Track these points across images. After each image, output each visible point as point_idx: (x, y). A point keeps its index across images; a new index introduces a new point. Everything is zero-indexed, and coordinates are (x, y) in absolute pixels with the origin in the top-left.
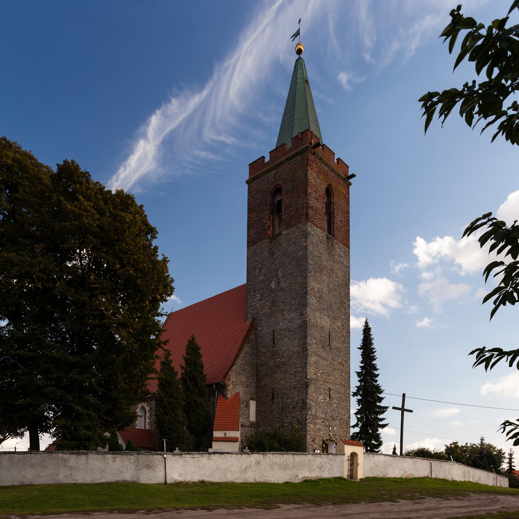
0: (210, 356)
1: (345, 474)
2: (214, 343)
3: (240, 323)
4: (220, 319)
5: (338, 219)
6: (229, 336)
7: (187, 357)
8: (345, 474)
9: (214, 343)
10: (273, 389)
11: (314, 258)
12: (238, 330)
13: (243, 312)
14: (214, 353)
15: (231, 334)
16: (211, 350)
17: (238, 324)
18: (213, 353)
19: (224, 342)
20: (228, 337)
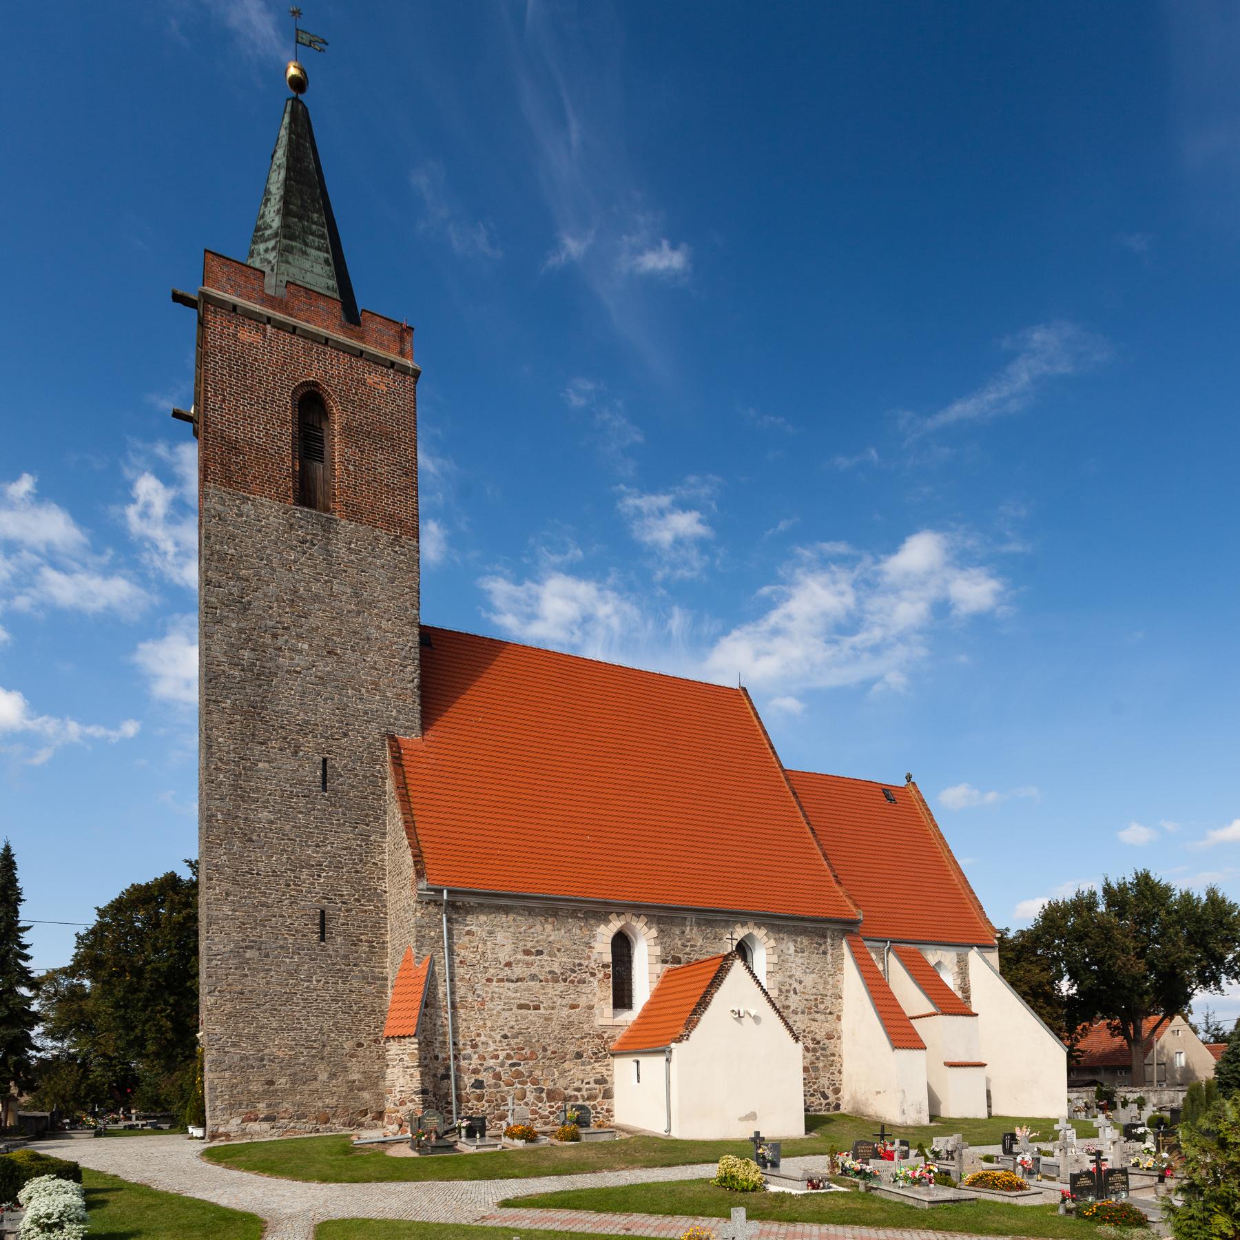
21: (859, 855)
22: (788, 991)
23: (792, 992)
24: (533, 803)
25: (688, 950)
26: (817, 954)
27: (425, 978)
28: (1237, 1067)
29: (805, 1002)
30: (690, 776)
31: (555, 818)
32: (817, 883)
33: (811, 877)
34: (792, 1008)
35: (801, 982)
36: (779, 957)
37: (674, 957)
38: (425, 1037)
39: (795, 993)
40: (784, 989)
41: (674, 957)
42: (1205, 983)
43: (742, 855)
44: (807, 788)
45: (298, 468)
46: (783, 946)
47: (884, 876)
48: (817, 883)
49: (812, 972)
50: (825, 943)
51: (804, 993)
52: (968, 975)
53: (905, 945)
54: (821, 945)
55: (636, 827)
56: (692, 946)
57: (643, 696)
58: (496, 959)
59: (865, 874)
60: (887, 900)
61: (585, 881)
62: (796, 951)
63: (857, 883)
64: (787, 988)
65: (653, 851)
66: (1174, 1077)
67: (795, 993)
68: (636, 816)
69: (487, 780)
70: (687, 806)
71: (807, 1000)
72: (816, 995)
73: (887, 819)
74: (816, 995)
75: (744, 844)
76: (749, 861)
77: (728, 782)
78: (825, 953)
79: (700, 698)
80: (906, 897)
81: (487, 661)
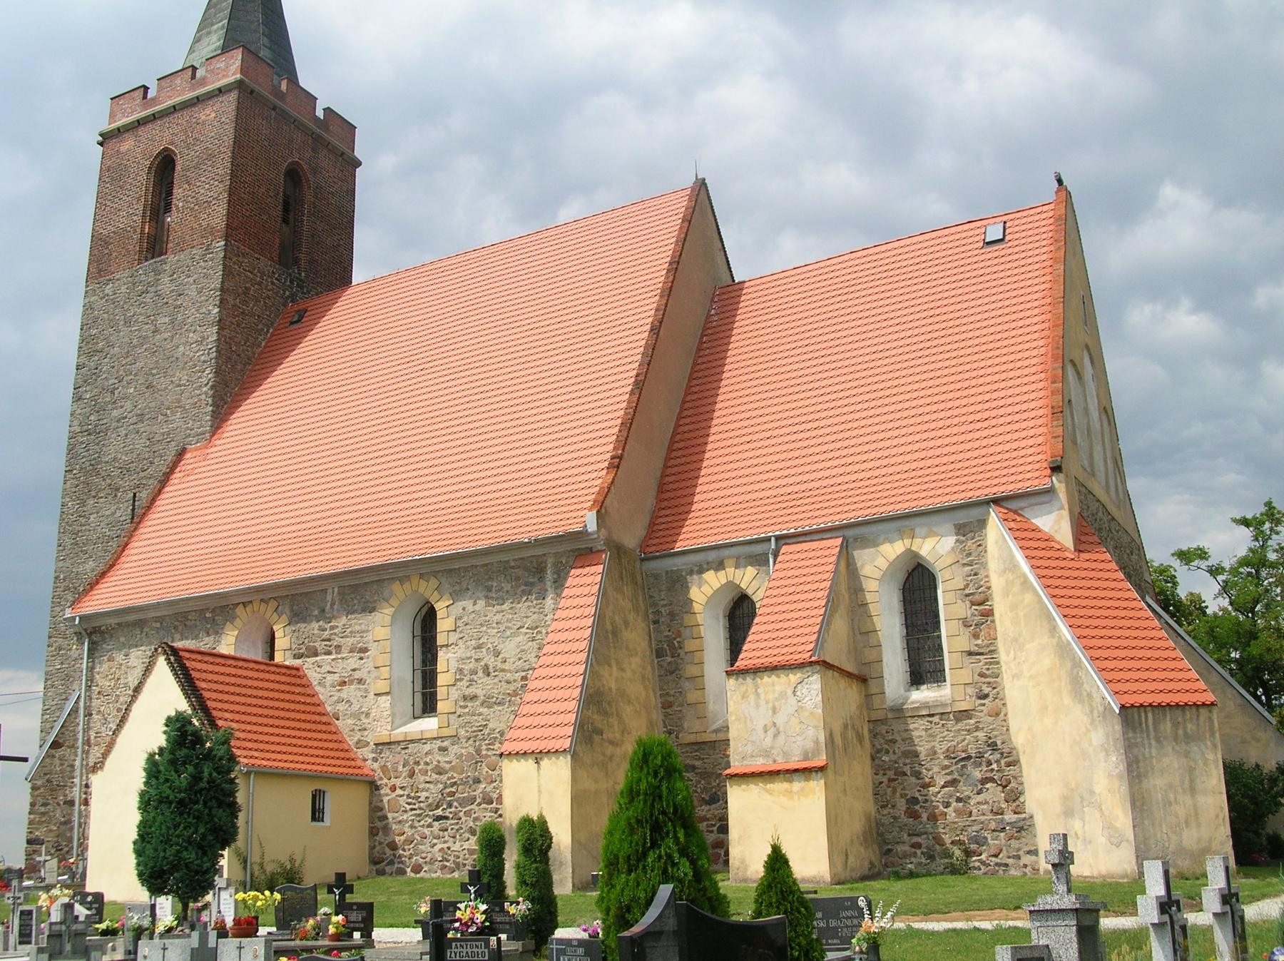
0: (238, 690)
1: (737, 765)
2: (900, 406)
3: (264, 557)
4: (939, 365)
5: (663, 416)
6: (325, 493)
7: (536, 894)
8: (737, 765)
9: (900, 406)
10: (1005, 223)
11: (159, 881)
12: (1037, 252)
13: (1031, 432)
14: (343, 360)
15: (526, 406)
16: (870, 421)
17: (582, 326)
18: (232, 689)
19: (262, 513)
20: (260, 494)
24: (1017, 417)
31: (985, 323)
32: (309, 375)
33: (750, 488)
42: (1202, 611)
43: (946, 372)
44: (322, 350)
48: (353, 325)
55: (542, 312)
59: (345, 349)
60: (224, 514)
61: (628, 319)
63: (780, 355)
65: (417, 341)
68: (502, 328)
69: (495, 302)
70: (870, 291)
73: (403, 344)
76: (370, 336)
79: (909, 283)
80: (897, 424)
81: (731, 301)
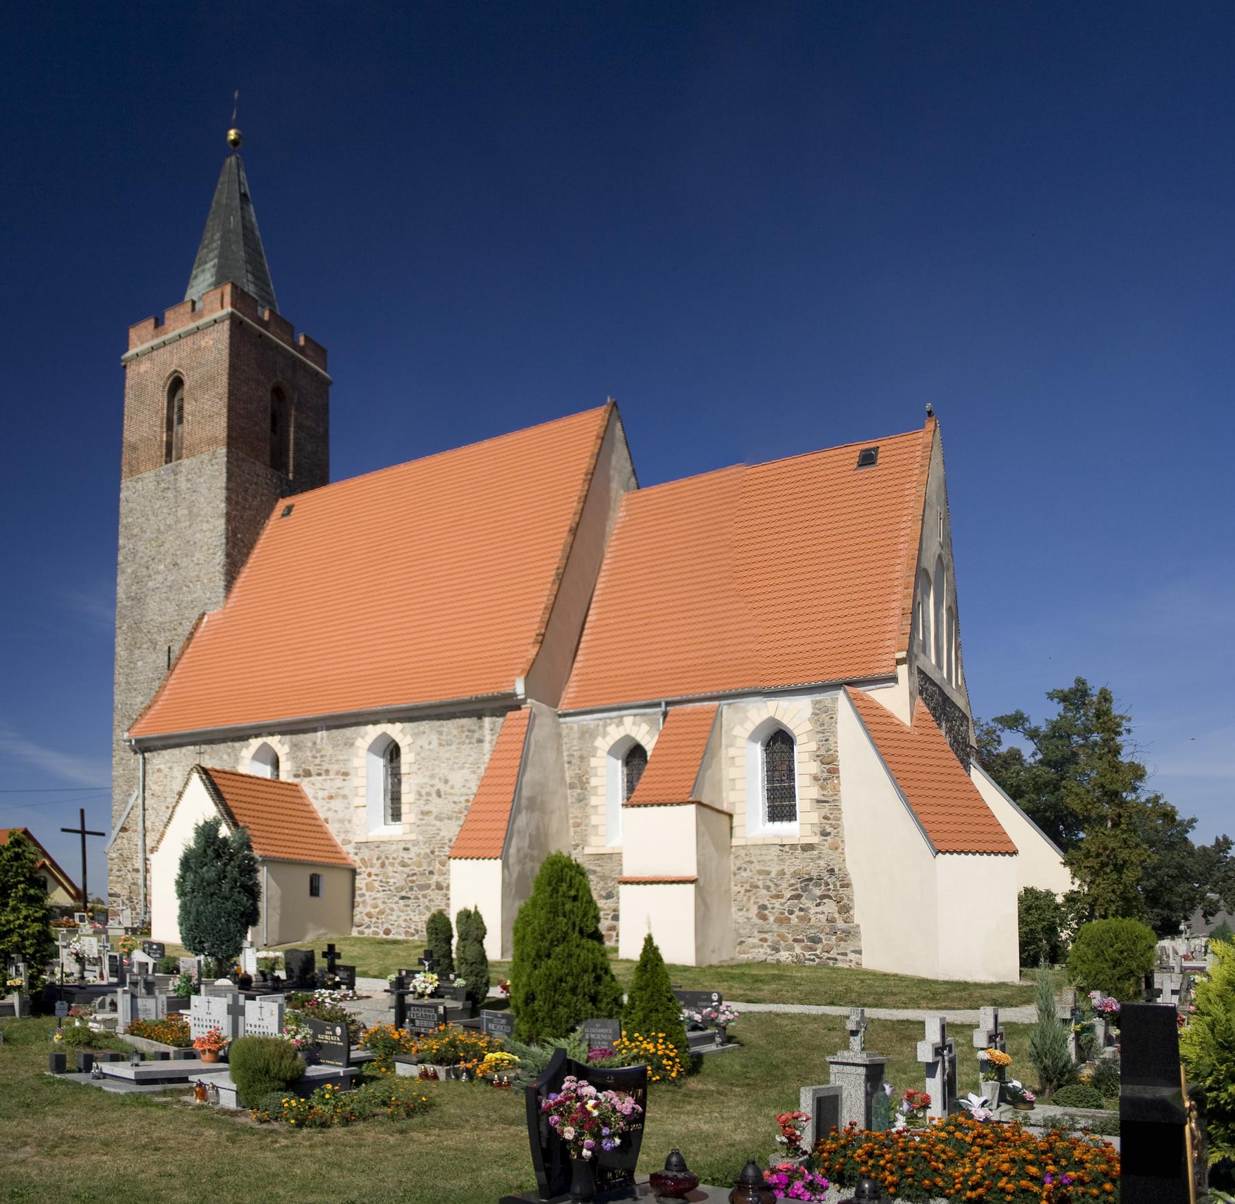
21: (529, 584)
22: (428, 794)
23: (434, 796)
25: (318, 761)
26: (470, 743)
27: (508, 813)
28: (4, 1068)
29: (453, 805)
30: (666, 586)
34: (435, 814)
35: (446, 782)
36: (418, 754)
37: (305, 771)
38: (121, 854)
39: (439, 794)
40: (424, 792)
41: (305, 771)
45: (165, 439)
46: (423, 741)
47: (490, 592)
49: (462, 768)
50: (481, 727)
51: (451, 794)
52: (834, 733)
53: (691, 705)
54: (474, 731)
56: (322, 756)
57: (716, 526)
58: (171, 790)
59: (694, 620)
62: (440, 745)
64: (428, 789)
66: (617, 1001)
67: (439, 794)
71: (455, 802)
72: (467, 795)
74: (467, 795)
75: (480, 630)
77: (675, 571)
78: (480, 741)
